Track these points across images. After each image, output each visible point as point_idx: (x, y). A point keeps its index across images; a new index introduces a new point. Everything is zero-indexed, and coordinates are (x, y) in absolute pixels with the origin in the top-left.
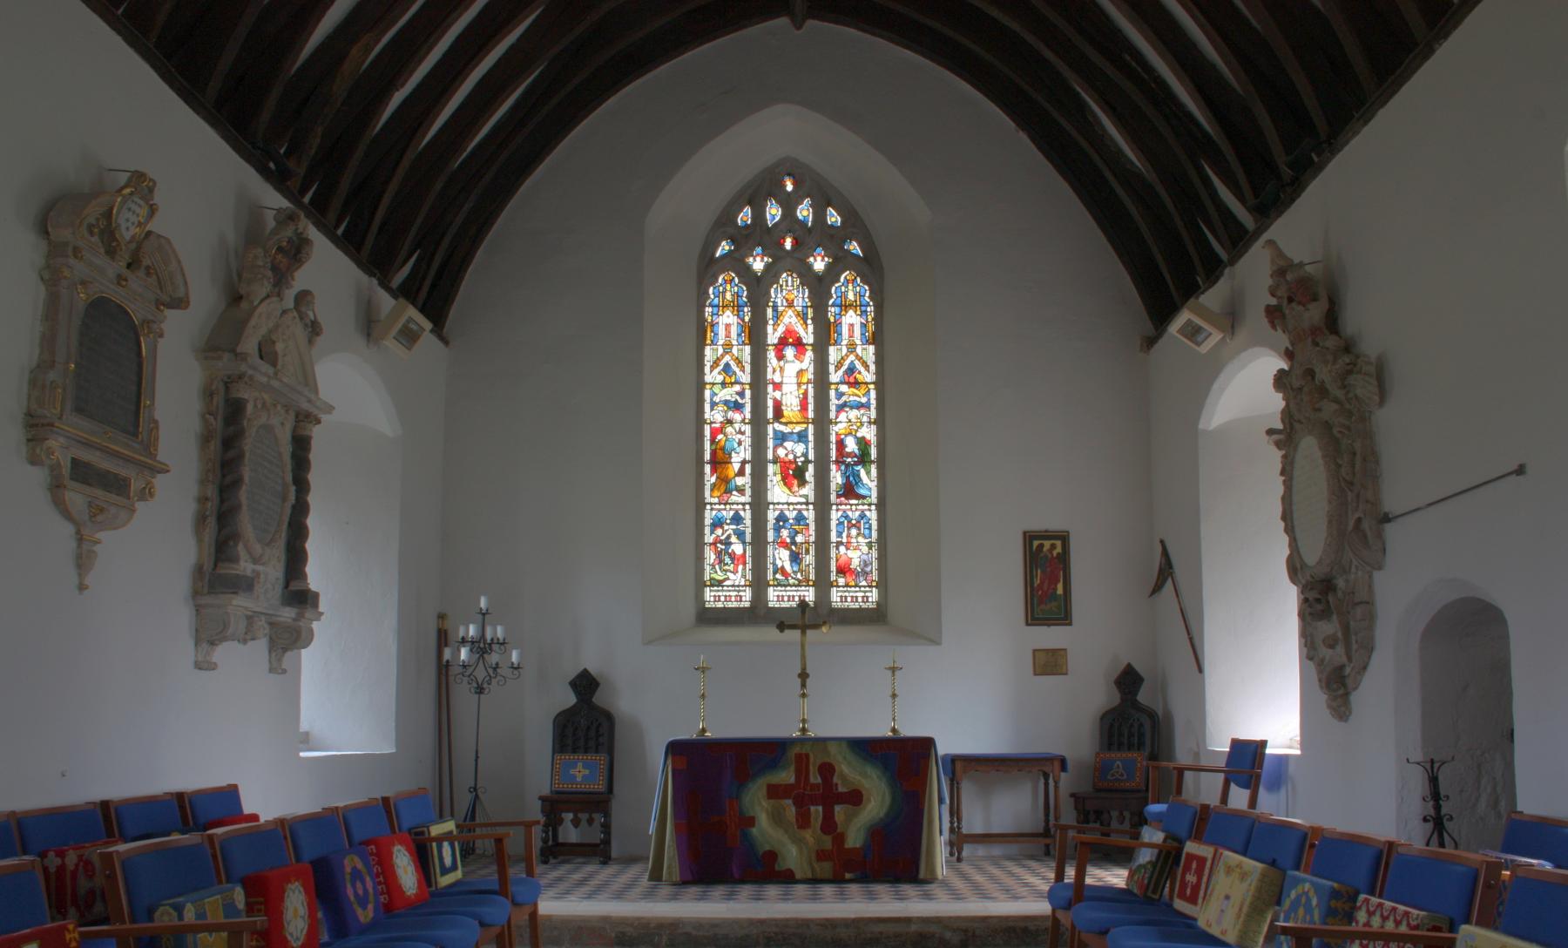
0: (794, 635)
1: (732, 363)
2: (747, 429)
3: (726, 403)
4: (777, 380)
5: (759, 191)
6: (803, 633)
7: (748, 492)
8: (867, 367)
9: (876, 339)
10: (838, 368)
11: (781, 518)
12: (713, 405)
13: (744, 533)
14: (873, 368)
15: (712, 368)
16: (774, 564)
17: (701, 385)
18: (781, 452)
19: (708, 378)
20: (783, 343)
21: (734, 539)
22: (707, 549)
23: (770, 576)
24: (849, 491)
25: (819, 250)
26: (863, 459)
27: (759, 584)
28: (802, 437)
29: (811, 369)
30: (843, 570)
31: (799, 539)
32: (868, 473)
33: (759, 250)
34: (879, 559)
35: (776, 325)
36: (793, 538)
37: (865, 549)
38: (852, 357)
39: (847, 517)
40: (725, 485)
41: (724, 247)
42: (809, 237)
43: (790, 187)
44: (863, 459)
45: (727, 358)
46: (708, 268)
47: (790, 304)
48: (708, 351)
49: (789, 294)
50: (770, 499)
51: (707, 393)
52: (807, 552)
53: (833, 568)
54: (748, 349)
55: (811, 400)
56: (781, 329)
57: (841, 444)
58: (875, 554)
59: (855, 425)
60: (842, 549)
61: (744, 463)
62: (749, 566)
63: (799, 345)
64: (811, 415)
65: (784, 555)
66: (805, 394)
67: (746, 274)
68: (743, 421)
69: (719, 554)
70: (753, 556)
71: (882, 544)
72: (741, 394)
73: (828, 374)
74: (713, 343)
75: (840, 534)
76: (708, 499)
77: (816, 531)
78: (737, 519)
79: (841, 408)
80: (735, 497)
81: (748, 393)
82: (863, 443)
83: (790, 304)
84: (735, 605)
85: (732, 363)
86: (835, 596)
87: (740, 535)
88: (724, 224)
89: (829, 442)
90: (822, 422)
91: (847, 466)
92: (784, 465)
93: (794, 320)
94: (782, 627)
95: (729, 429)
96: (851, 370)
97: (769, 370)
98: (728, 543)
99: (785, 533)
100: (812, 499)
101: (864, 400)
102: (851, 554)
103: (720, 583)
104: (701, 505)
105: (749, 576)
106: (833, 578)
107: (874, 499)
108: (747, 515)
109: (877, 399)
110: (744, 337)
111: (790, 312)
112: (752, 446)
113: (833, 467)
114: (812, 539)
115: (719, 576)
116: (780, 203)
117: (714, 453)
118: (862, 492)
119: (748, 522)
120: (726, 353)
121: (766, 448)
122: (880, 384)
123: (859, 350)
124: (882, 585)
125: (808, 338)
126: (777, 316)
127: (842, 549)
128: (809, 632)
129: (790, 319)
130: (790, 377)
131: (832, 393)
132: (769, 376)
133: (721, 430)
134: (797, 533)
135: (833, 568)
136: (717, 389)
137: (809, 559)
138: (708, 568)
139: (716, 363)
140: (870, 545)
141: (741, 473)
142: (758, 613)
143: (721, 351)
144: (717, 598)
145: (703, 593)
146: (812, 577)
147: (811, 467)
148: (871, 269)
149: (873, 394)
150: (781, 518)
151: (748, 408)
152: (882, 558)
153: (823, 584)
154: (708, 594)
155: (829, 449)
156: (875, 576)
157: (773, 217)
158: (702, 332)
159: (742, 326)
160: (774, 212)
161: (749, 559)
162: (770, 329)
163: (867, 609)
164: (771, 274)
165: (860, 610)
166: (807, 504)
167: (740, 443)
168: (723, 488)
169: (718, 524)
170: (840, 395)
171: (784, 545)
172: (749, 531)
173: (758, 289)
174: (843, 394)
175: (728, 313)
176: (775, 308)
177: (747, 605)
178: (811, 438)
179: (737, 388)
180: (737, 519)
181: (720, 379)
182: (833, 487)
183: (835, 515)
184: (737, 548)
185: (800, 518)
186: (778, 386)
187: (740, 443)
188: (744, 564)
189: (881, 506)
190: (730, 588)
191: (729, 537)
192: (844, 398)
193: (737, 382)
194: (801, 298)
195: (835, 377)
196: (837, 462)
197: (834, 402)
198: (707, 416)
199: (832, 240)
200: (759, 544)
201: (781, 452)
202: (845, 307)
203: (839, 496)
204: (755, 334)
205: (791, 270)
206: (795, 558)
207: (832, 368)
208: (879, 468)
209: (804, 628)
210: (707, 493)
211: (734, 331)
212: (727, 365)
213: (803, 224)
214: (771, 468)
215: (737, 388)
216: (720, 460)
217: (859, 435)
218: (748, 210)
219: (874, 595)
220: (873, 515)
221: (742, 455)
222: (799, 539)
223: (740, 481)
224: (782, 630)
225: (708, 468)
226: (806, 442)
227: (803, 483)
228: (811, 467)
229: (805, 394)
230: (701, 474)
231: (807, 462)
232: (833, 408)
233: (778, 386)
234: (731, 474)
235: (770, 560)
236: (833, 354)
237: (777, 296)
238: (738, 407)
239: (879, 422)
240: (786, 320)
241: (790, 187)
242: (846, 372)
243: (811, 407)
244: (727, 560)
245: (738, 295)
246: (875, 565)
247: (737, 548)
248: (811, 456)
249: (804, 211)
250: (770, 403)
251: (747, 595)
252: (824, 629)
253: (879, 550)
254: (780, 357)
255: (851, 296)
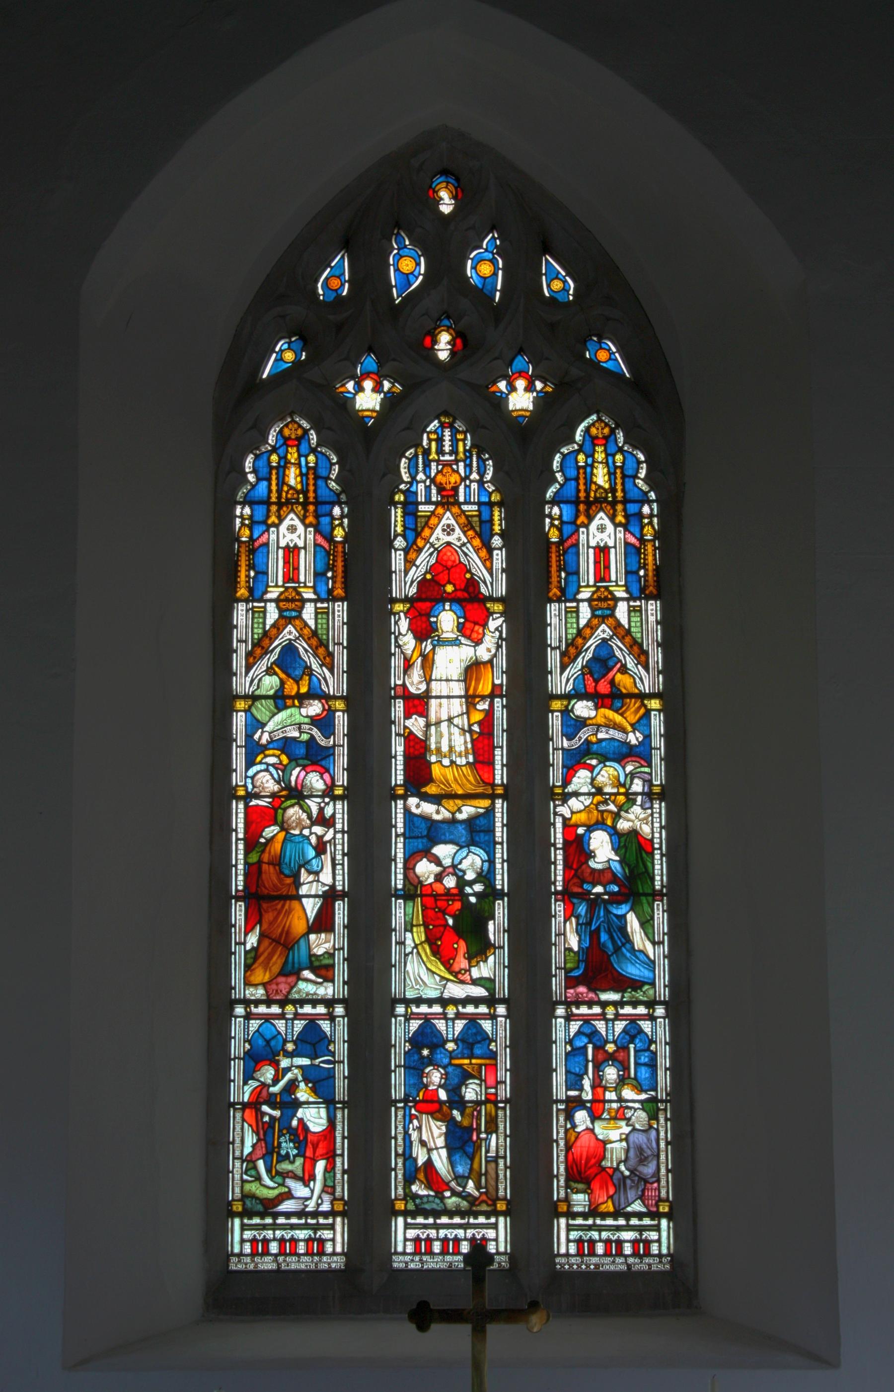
0: (451, 1340)
1: (302, 646)
2: (339, 811)
3: (286, 745)
4: (415, 684)
5: (367, 218)
6: (479, 1332)
7: (341, 971)
8: (642, 656)
9: (663, 583)
10: (567, 658)
11: (426, 1038)
12: (254, 751)
13: (330, 1076)
14: (656, 656)
15: (251, 659)
16: (408, 1157)
17: (223, 702)
18: (425, 869)
19: (242, 684)
20: (428, 596)
21: (303, 1093)
22: (235, 1117)
23: (396, 1190)
24: (599, 968)
25: (520, 362)
26: (632, 886)
27: (368, 1210)
28: (477, 832)
29: (502, 662)
30: (587, 1170)
31: (471, 1092)
32: (646, 923)
33: (370, 362)
34: (675, 1143)
35: (412, 550)
36: (455, 1092)
37: (640, 1117)
38: (604, 631)
39: (593, 1035)
40: (283, 954)
41: (284, 355)
42: (500, 329)
43: (447, 207)
44: (632, 886)
45: (290, 632)
46: (241, 408)
47: (448, 499)
48: (240, 614)
49: (446, 514)
50: (395, 989)
51: (239, 721)
52: (492, 1127)
53: (559, 1167)
54: (340, 610)
55: (500, 738)
56: (424, 560)
57: (577, 849)
58: (664, 1130)
59: (610, 805)
60: (581, 1117)
61: (330, 897)
62: (341, 1163)
63: (470, 600)
64: (500, 775)
65: (434, 1131)
66: (488, 721)
67: (337, 420)
68: (329, 793)
69: (264, 1131)
70: (352, 1138)
71: (683, 1105)
72: (324, 723)
73: (545, 672)
74: (255, 595)
75: (574, 1081)
76: (240, 990)
77: (514, 1071)
78: (312, 1041)
79: (576, 760)
80: (308, 985)
81: (341, 720)
82: (631, 845)
83: (448, 499)
84: (305, 1263)
85: (619, 649)
86: (564, 1239)
87: (321, 1083)
88: (280, 296)
89: (549, 845)
90: (530, 795)
91: (594, 903)
92: (431, 901)
93: (457, 536)
94: (423, 1316)
95: (294, 813)
96: (603, 662)
97: (397, 663)
98: (289, 1104)
99: (435, 1077)
100: (503, 989)
101: (633, 738)
102: (600, 1130)
103: (268, 1207)
104: (220, 1006)
105: (343, 1190)
106: (558, 1191)
107: (663, 993)
108: (338, 1031)
109: (668, 736)
110: (333, 581)
111: (448, 519)
112: (351, 854)
113: (558, 908)
114: (505, 1092)
115: (267, 1188)
116: (425, 246)
117: (253, 872)
118: (633, 970)
119: (341, 1049)
120: (284, 620)
121: (391, 860)
122: (673, 697)
123: (621, 612)
124: (683, 1212)
125: (493, 578)
126: (416, 529)
127: (581, 1117)
128: (493, 1330)
129: (447, 532)
130: (449, 674)
131: (555, 722)
132: (396, 680)
133: (273, 815)
134: (466, 1076)
135: (559, 1167)
136: (261, 710)
137: (495, 1143)
138: (237, 1167)
139: (260, 647)
140: (651, 1107)
141: (323, 922)
142: (363, 1285)
143: (272, 614)
144: (260, 1248)
145: (224, 1232)
146: (504, 1189)
147: (501, 909)
148: (650, 408)
149: (657, 723)
150: (426, 1038)
151: (342, 759)
152: (683, 1142)
153: (532, 1211)
154: (238, 1236)
155: (548, 863)
156: (666, 1189)
157: (407, 278)
158: (227, 567)
159: (327, 547)
160: (407, 267)
161: (341, 1144)
162: (397, 560)
163: (648, 1276)
164: (398, 426)
165: (629, 1274)
166: (491, 1001)
167: (320, 848)
168: (277, 963)
169: (263, 1053)
170: (575, 725)
171: (431, 1106)
172: (342, 1070)
173: (367, 461)
174: (582, 723)
175: (292, 519)
176: (410, 507)
177: (338, 1263)
178: (500, 833)
179: (315, 708)
180: (312, 1041)
181: (270, 683)
182: (557, 957)
183: (562, 1030)
184: (314, 1118)
185: (473, 1039)
186: (418, 704)
187: (320, 848)
188: (331, 1157)
189: (679, 1008)
190: (298, 1217)
191: (292, 1086)
192: (584, 734)
193: (314, 694)
194: (476, 483)
195: (561, 681)
196: (567, 895)
197: (559, 743)
198: (236, 779)
199: (553, 339)
200: (367, 1108)
201: (425, 869)
202: (588, 504)
203: (571, 982)
204: (358, 572)
205: (448, 414)
206: (460, 1141)
207: (553, 659)
208: (672, 912)
209: (480, 1319)
210: (237, 975)
211: (306, 564)
212: (289, 649)
213: (481, 295)
214: (399, 912)
215: (315, 708)
216: (270, 891)
217: (623, 825)
218: (341, 263)
219: (663, 1238)
220: (658, 1030)
221: (326, 877)
222: (471, 1092)
223: (320, 944)
224: (423, 1327)
225: (238, 913)
226: (489, 847)
227: (481, 948)
228: (501, 909)
229: (488, 721)
230: (224, 926)
231: (491, 894)
232: (557, 759)
233: (418, 704)
234: (299, 926)
235: (396, 1146)
236: (557, 623)
237: (415, 478)
238: (314, 756)
239: (673, 794)
240: (439, 537)
241: (447, 207)
242: (587, 669)
243: (500, 757)
244: (288, 1147)
245: (313, 475)
246: (666, 1158)
247: (314, 1118)
248: (501, 880)
249: (483, 267)
250: (398, 748)
251: (337, 1238)
252: (536, 1320)
253: (675, 1120)
254: (424, 630)
255: (601, 477)
